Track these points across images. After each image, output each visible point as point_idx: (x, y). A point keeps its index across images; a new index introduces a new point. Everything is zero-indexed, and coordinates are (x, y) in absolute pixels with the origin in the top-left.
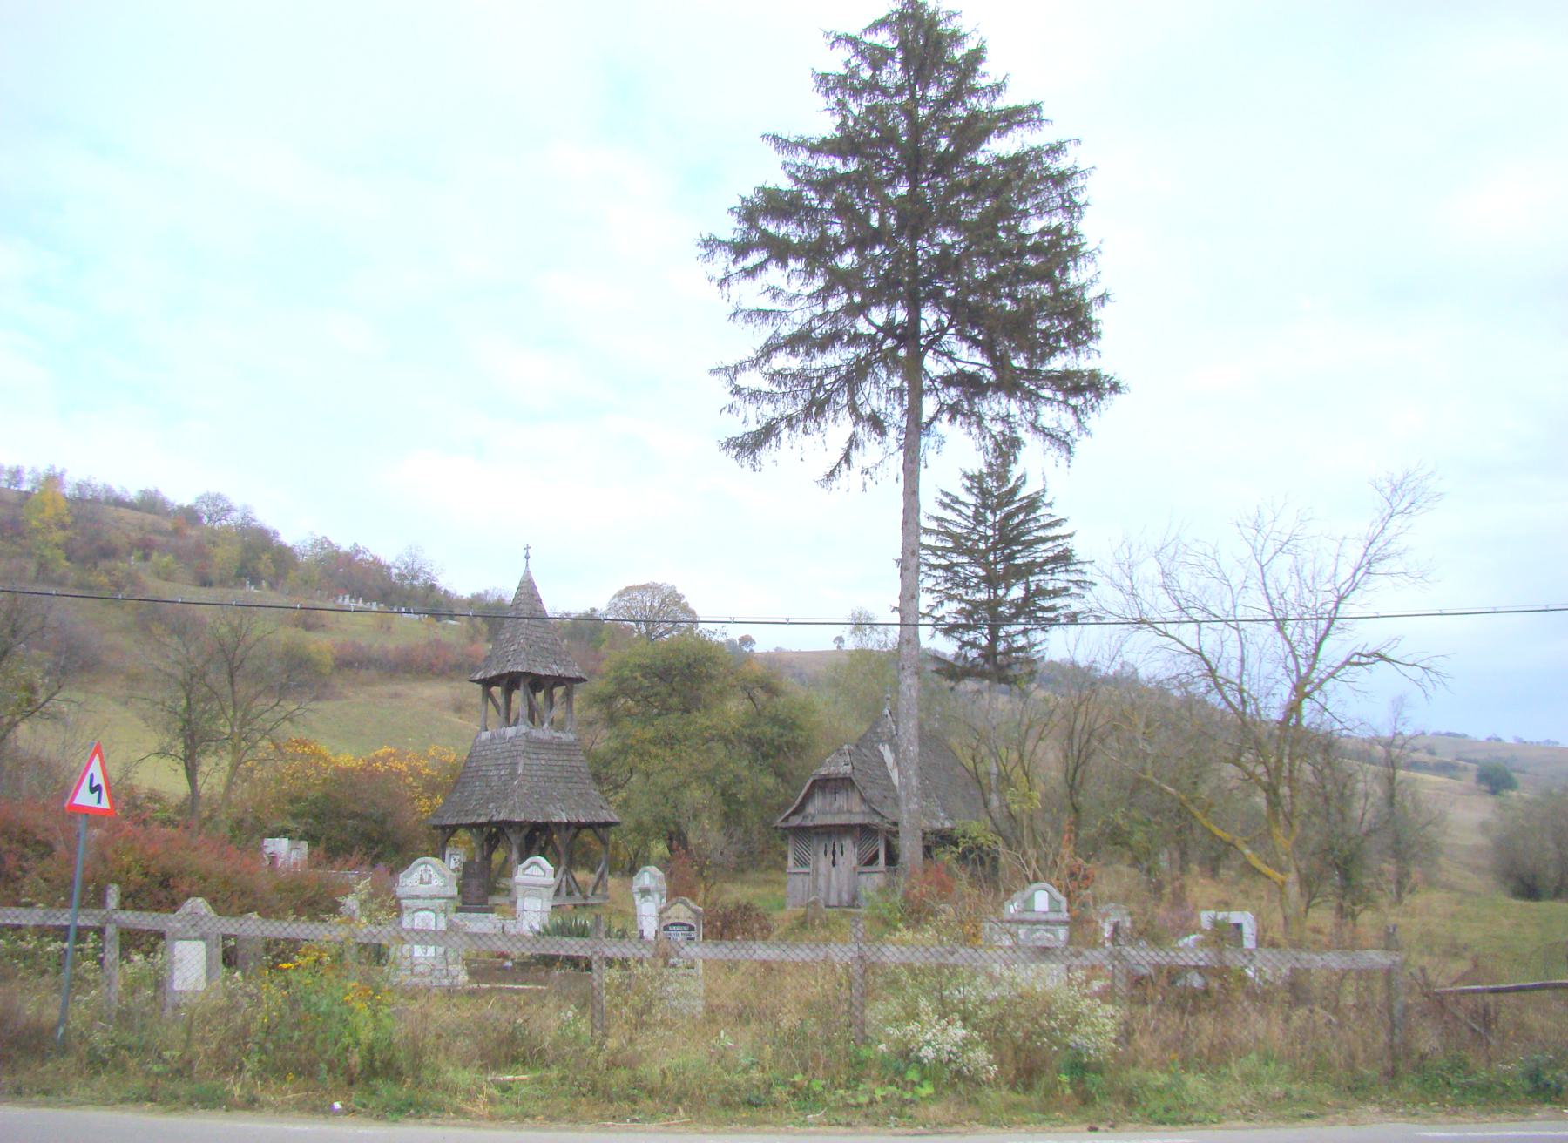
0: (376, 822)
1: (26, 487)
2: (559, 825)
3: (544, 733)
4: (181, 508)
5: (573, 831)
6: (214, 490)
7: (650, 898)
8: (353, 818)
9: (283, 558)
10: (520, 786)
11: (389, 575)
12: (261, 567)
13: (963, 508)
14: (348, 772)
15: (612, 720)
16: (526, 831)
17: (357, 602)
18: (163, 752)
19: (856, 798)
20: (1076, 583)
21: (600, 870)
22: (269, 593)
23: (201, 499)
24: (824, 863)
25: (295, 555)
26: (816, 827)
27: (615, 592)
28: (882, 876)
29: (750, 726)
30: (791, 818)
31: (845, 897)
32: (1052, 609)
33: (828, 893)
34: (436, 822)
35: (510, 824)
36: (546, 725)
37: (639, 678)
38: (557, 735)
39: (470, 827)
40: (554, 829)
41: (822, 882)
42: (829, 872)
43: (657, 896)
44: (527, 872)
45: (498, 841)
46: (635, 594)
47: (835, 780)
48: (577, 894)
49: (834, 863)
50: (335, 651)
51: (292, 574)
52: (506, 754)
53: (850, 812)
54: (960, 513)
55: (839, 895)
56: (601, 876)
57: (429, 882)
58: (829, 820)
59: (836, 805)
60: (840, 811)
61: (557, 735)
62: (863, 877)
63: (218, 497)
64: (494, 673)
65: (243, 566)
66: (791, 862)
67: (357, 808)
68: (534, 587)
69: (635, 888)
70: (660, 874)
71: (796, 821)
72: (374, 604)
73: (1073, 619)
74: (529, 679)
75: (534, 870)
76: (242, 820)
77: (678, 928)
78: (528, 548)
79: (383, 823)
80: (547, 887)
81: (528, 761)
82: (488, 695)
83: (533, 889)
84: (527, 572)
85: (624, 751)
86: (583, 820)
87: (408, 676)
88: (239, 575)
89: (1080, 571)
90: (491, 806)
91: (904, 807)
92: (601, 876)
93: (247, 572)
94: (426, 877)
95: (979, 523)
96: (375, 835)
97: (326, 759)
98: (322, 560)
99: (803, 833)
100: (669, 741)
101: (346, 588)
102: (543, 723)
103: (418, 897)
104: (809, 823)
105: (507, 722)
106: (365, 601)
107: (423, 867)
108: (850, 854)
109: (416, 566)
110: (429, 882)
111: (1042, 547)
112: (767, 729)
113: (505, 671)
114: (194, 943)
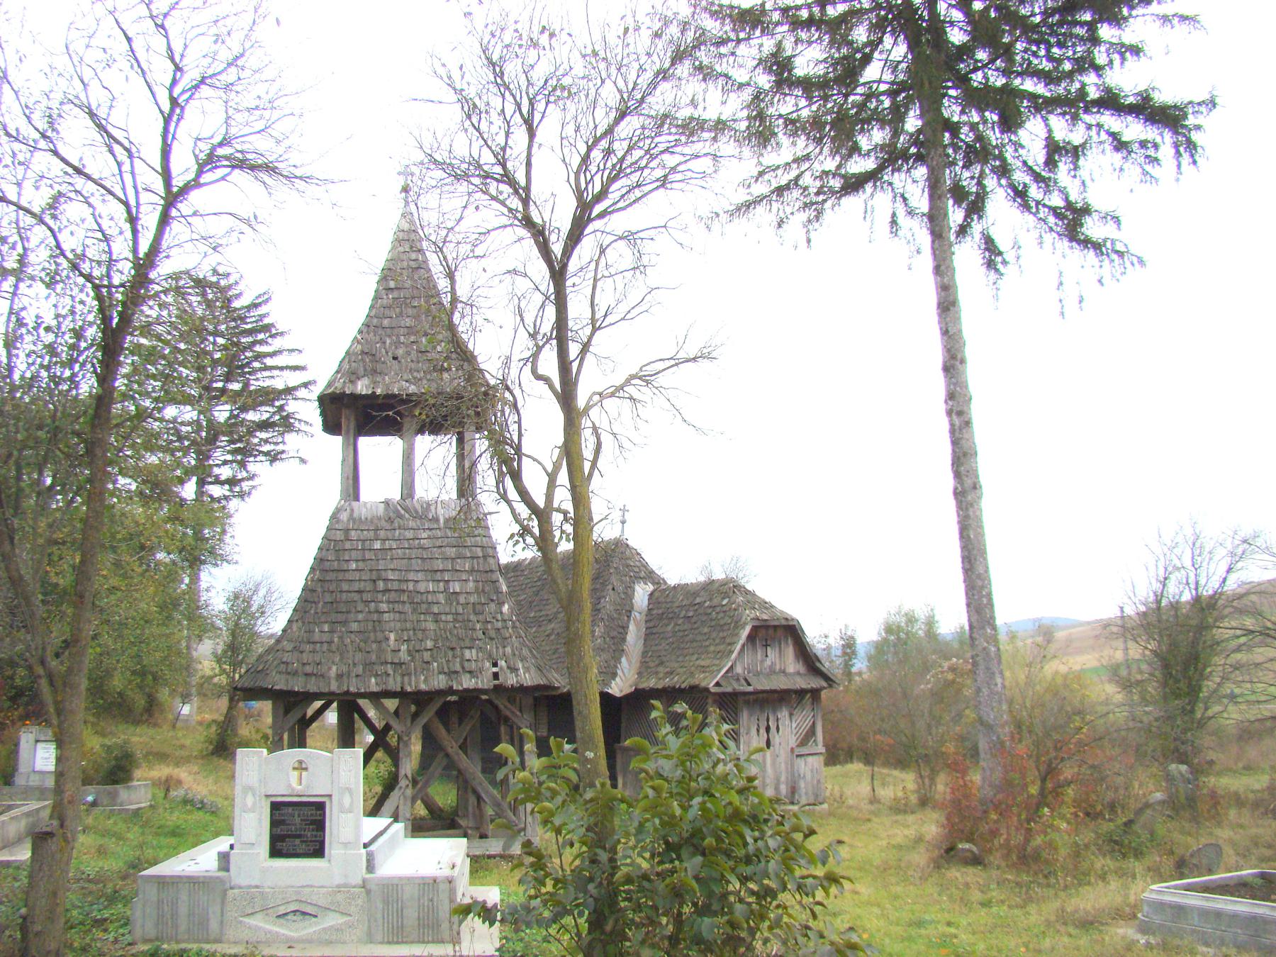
31: (783, 789)
52: (451, 552)
59: (768, 662)
62: (801, 762)
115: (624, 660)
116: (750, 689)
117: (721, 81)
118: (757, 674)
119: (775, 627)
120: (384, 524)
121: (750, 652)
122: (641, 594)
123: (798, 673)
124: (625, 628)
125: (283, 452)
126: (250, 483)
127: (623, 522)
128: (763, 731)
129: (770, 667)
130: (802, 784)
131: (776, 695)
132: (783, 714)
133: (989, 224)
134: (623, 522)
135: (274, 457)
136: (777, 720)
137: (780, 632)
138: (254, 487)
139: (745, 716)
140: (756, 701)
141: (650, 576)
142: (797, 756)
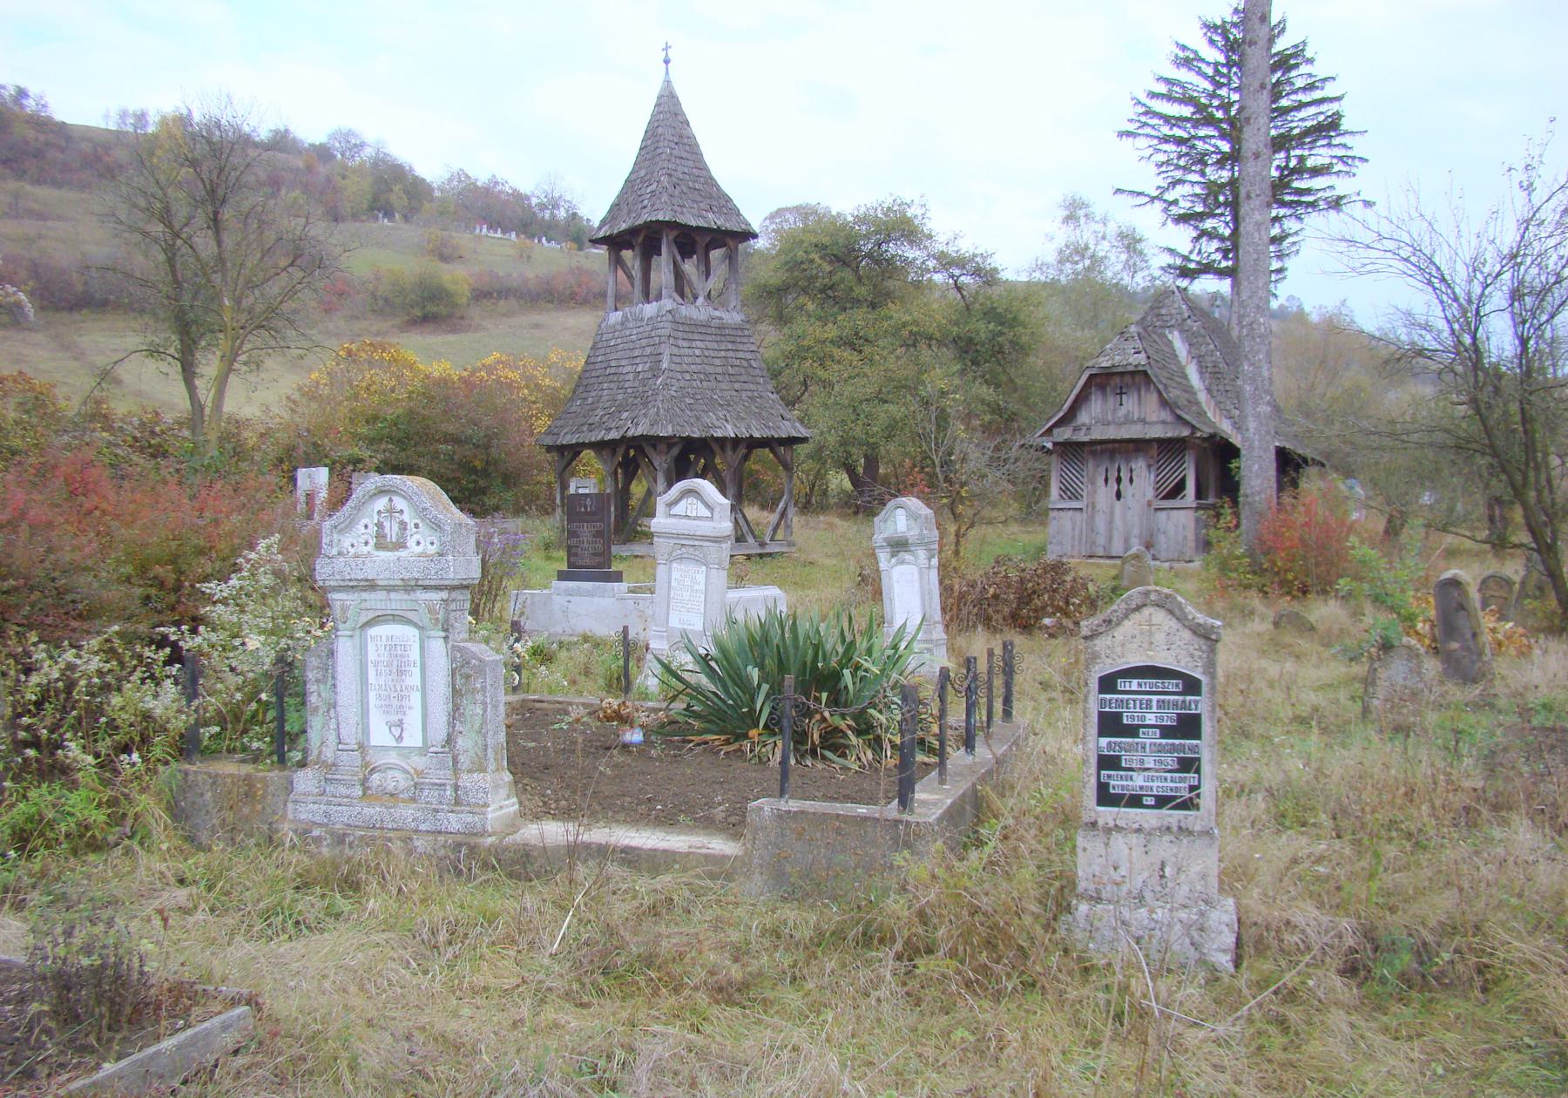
0: (477, 446)
1: (151, 129)
2: (722, 441)
3: (698, 311)
4: (312, 145)
5: (742, 451)
6: (345, 124)
7: (907, 557)
8: (446, 442)
9: (416, 190)
10: (666, 385)
11: (530, 206)
12: (393, 198)
13: (1203, 66)
14: (444, 382)
15: (782, 319)
16: (675, 451)
17: (496, 232)
18: (154, 352)
19: (1152, 399)
20: (1340, 158)
21: (781, 505)
22: (403, 226)
23: (333, 137)
24: (1104, 494)
25: (433, 190)
26: (1093, 443)
27: (767, 214)
28: (1191, 514)
29: (956, 323)
30: (1055, 431)
32: (1308, 191)
33: (1110, 539)
34: (549, 441)
35: (654, 441)
36: (701, 300)
37: (817, 259)
38: (717, 314)
39: (599, 446)
40: (716, 448)
43: (922, 554)
44: (679, 509)
45: (637, 467)
46: (788, 216)
47: (1122, 374)
48: (751, 540)
49: (1118, 495)
50: (471, 281)
51: (427, 206)
52: (644, 342)
53: (1143, 421)
54: (1200, 73)
55: (1127, 541)
56: (783, 514)
57: (400, 545)
58: (1112, 433)
59: (1122, 412)
60: (1128, 420)
61: (717, 314)
62: (1162, 515)
63: (350, 133)
64: (624, 226)
65: (375, 199)
66: (1054, 491)
67: (450, 428)
68: (678, 104)
69: (879, 538)
70: (926, 511)
71: (1064, 434)
72: (513, 235)
73: (1336, 204)
74: (674, 234)
75: (689, 506)
76: (294, 448)
77: (1148, 684)
78: (667, 48)
79: (487, 447)
80: (717, 540)
81: (676, 351)
82: (617, 262)
83: (690, 546)
84: (668, 83)
85: (800, 354)
86: (757, 435)
87: (551, 306)
88: (372, 209)
89: (1344, 146)
90: (625, 415)
91: (1249, 410)
92: (783, 514)
93: (379, 206)
94: (391, 530)
95: (1219, 85)
96: (478, 464)
97: (411, 367)
98: (460, 194)
99: (1071, 451)
100: (853, 342)
101: (484, 219)
102: (696, 298)
103: (371, 586)
104: (1082, 437)
105: (647, 297)
106: (504, 232)
107: (381, 503)
108: (1143, 480)
109: (556, 195)
110: (400, 545)
111: (1303, 114)
112: (981, 325)
113: (640, 221)
114: (476, 561)
120: (619, 327)
121: (1099, 402)
125: (1340, 198)
127: (667, 62)
129: (1126, 416)
130: (1162, 539)
131: (1131, 446)
134: (667, 62)
136: (1131, 471)
140: (1103, 452)
142: (1156, 509)
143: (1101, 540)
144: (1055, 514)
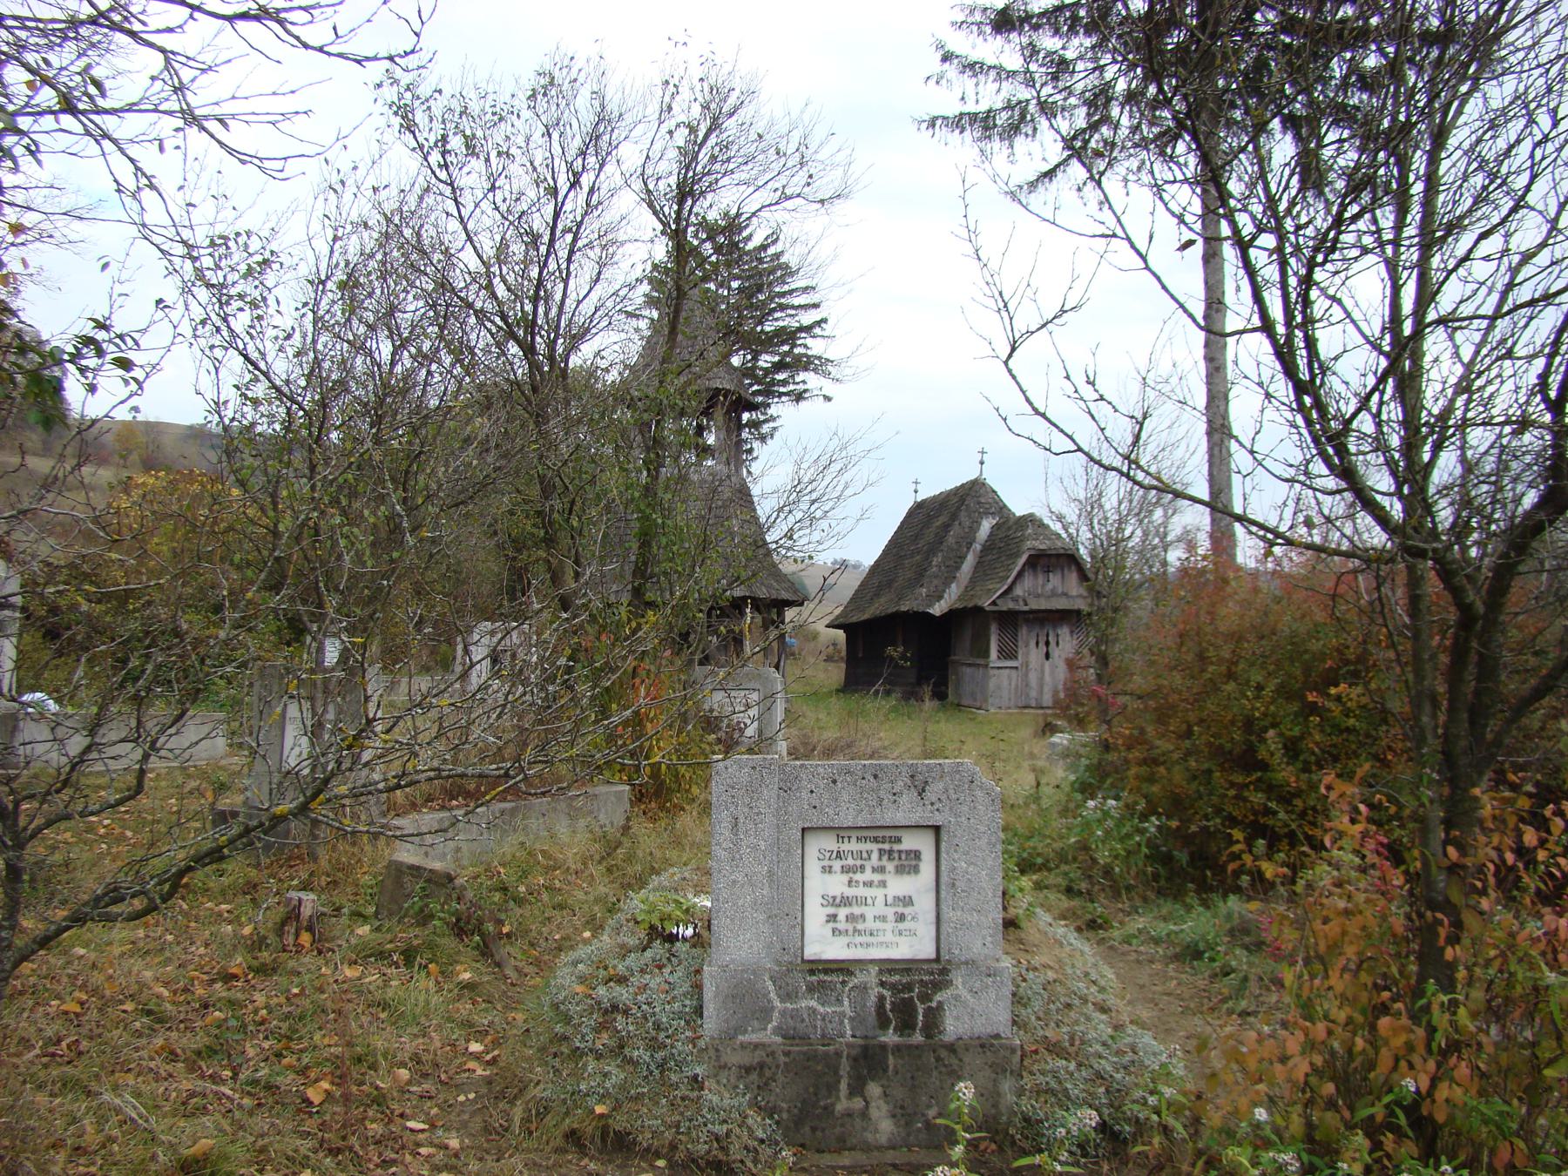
33: (1041, 692)
41: (1033, 678)
42: (1042, 666)
59: (1050, 586)
115: (953, 586)
116: (1026, 608)
117: (993, 74)
118: (1038, 596)
119: (1058, 556)
122: (986, 526)
123: (1080, 596)
124: (963, 558)
125: (805, 391)
126: (772, 425)
127: (982, 463)
128: (1042, 644)
132: (1064, 632)
133: (168, 746)
134: (982, 463)
135: (799, 397)
137: (1053, 560)
138: (775, 429)
139: (1023, 632)
141: (1002, 509)
143: (1033, 694)
144: (996, 672)
